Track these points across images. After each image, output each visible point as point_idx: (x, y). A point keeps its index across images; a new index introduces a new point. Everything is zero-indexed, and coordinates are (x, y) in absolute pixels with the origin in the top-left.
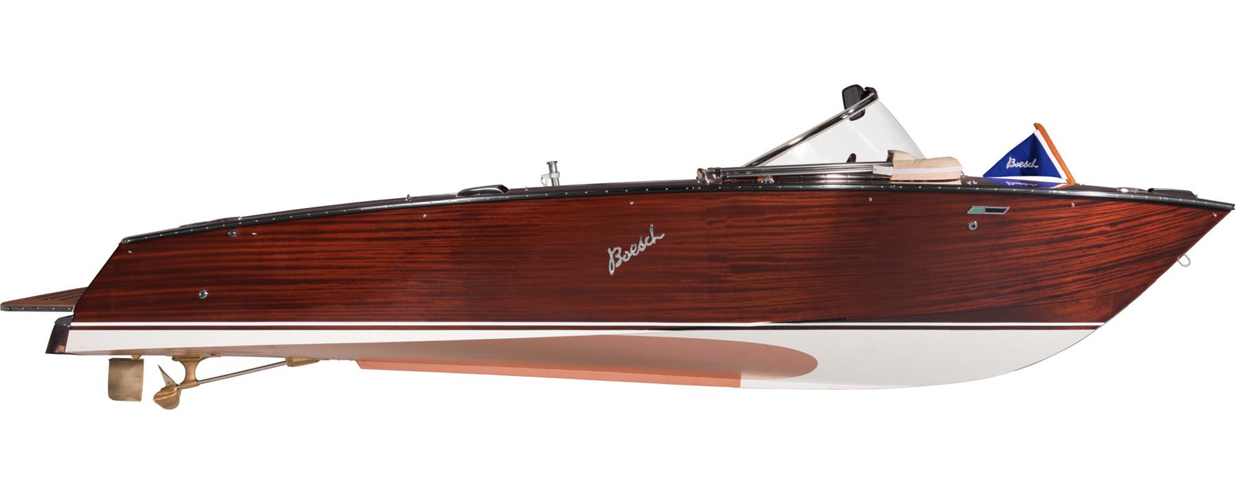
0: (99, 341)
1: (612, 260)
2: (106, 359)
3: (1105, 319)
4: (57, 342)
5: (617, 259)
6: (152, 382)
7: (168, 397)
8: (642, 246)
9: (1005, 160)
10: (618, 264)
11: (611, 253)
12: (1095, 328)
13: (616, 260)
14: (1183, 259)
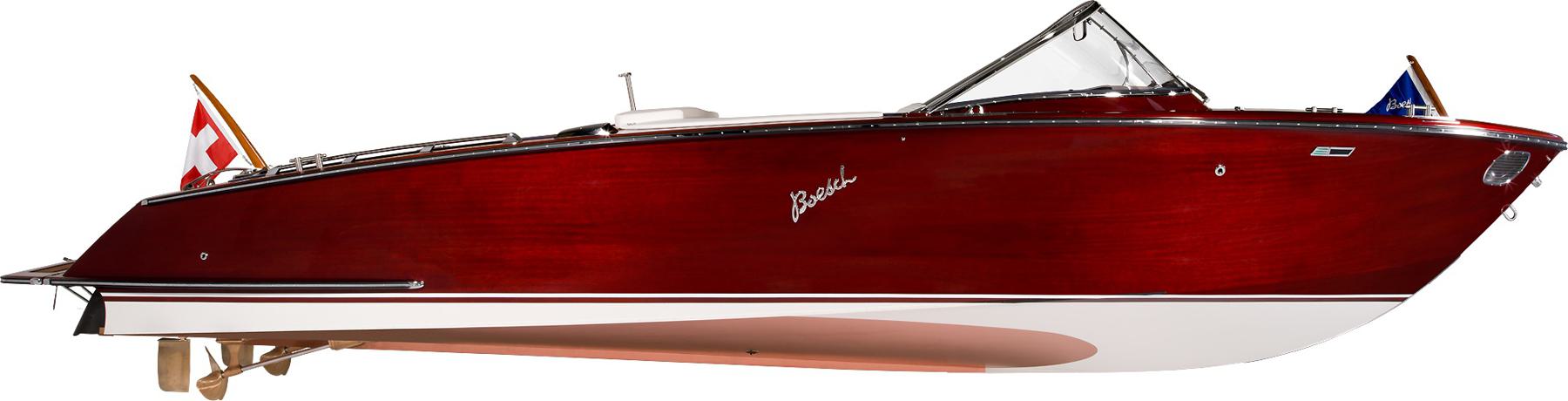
0: (140, 319)
1: (795, 205)
2: (154, 343)
3: (1413, 291)
4: (92, 322)
5: (801, 204)
6: (199, 367)
7: (215, 384)
8: (832, 189)
9: (597, 127)
10: (802, 210)
11: (794, 198)
12: (1403, 300)
13: (800, 205)
14: (1509, 212)
